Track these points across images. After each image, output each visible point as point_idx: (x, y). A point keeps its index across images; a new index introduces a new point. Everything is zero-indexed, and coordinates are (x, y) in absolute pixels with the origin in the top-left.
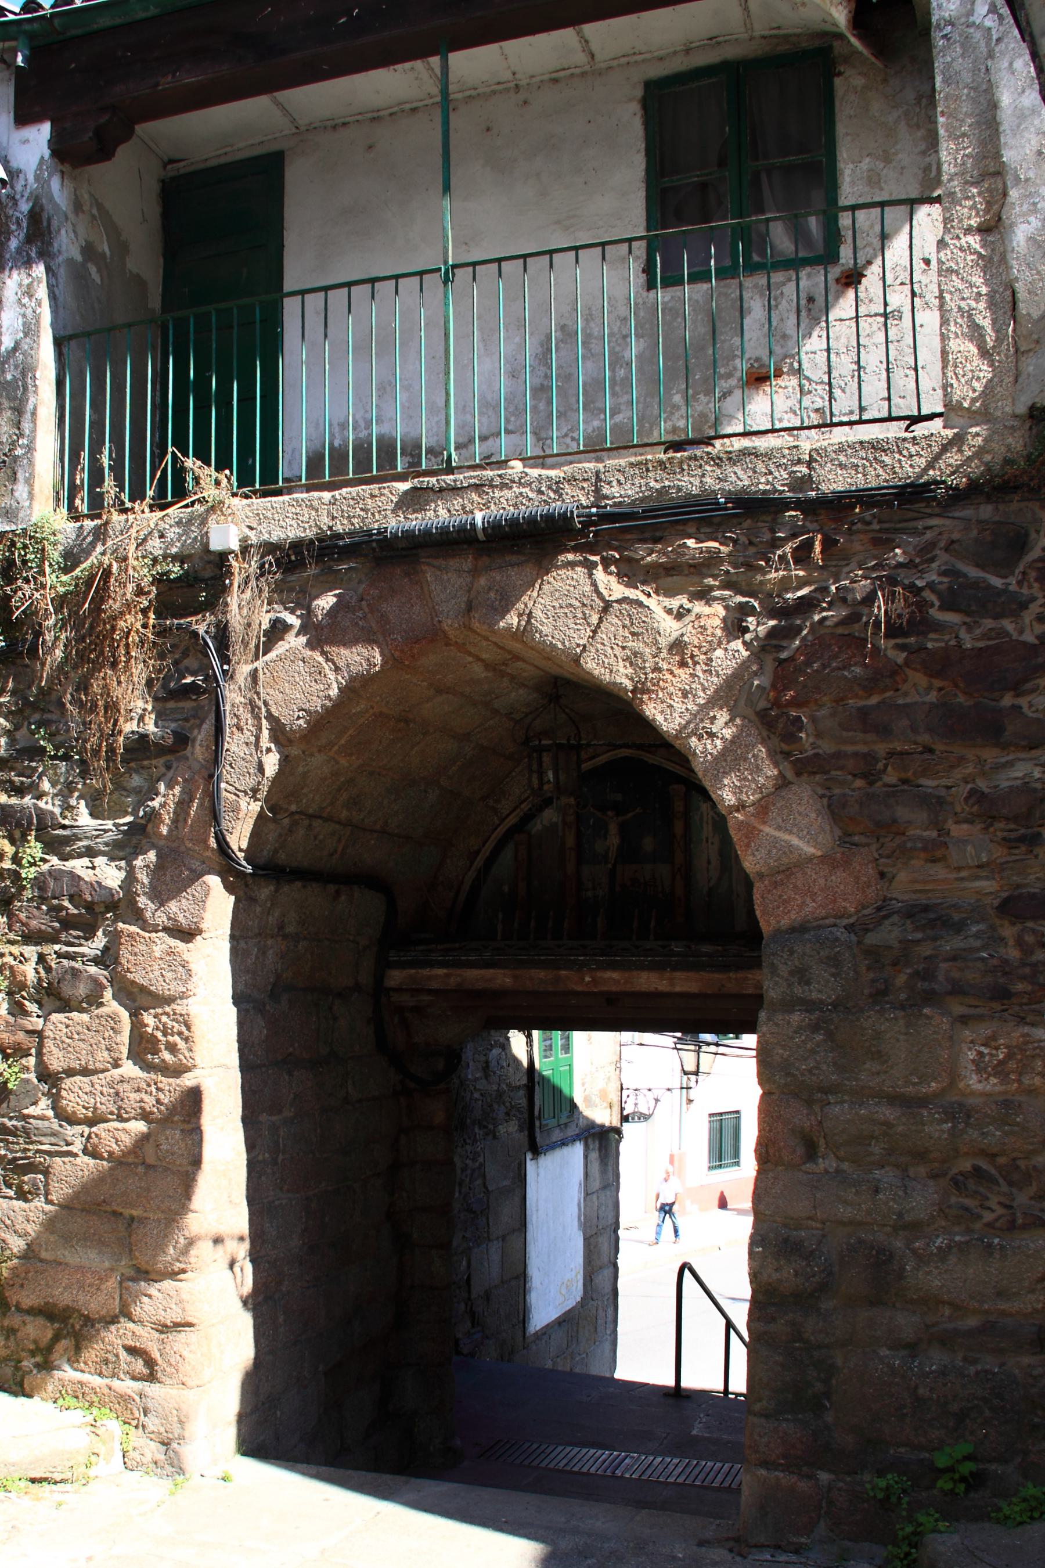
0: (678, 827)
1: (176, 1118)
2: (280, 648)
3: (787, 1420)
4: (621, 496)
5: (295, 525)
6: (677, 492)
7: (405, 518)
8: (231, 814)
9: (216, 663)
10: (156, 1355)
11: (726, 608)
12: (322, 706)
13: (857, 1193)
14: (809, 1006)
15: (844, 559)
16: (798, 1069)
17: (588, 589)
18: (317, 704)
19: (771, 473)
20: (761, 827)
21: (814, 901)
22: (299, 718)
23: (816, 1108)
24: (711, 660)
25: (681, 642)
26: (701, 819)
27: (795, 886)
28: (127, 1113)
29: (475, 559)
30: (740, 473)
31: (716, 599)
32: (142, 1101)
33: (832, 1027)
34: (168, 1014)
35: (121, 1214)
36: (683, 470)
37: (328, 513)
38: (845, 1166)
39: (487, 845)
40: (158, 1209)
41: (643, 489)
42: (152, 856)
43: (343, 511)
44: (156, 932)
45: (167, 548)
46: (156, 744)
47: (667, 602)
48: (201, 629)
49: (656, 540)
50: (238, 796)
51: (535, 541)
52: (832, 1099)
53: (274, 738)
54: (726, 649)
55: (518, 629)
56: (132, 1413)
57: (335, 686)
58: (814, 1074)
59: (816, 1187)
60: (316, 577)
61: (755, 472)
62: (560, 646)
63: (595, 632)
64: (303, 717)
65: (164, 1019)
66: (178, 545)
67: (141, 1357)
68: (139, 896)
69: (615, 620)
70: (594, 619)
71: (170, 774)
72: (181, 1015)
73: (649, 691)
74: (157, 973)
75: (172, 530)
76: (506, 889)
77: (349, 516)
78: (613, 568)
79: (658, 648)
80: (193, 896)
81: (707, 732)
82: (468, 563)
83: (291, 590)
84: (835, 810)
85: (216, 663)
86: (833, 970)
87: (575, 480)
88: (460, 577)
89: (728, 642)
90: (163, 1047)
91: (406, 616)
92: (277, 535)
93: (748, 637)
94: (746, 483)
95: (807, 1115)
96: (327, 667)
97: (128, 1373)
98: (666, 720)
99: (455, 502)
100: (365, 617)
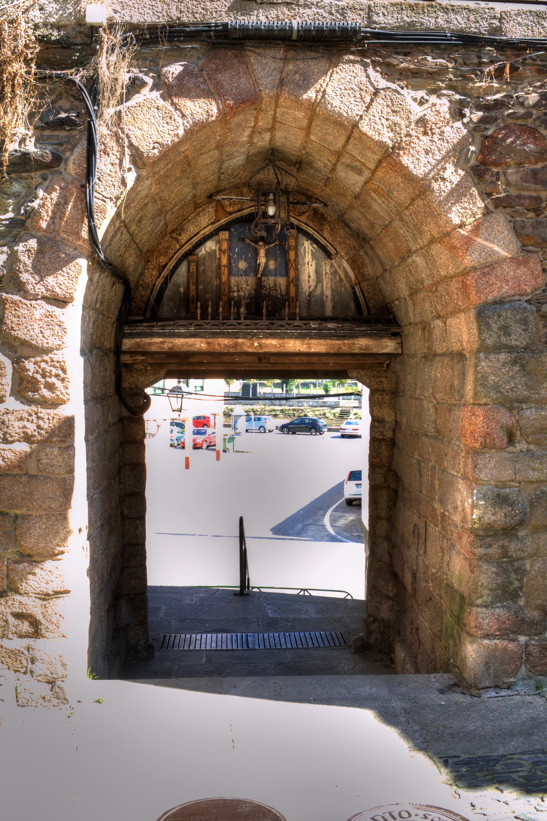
0: (292, 254)
1: (55, 439)
2: (137, 99)
3: (498, 607)
4: (385, 23)
5: (151, 14)
6: (421, 26)
7: (235, 18)
8: (99, 214)
9: (89, 103)
10: (39, 617)
11: (450, 101)
12: (172, 141)
13: (541, 463)
14: (510, 349)
15: (520, 80)
16: (504, 388)
17: (364, 79)
18: (168, 140)
19: (478, 22)
20: (475, 239)
21: (507, 285)
22: (154, 148)
23: (515, 412)
24: (443, 132)
25: (424, 119)
26: (305, 251)
27: (496, 276)
28: (11, 436)
29: (286, 52)
30: (460, 20)
31: (444, 95)
32: (24, 427)
33: (525, 362)
34: (46, 362)
35: (7, 514)
36: (424, 12)
37: (177, 8)
38: (532, 447)
40: (40, 508)
41: (399, 20)
42: (33, 243)
43: (188, 8)
44: (36, 300)
45: (46, 18)
46: (36, 161)
47: (413, 93)
48: (77, 79)
49: (406, 54)
50: (105, 202)
51: (330, 43)
52: (524, 406)
53: (134, 161)
54: (452, 127)
55: (315, 100)
56: (21, 663)
57: (182, 127)
58: (514, 391)
59: (516, 461)
60: (166, 51)
61: (469, 20)
62: (345, 115)
63: (368, 108)
64: (158, 148)
65: (43, 365)
66: (56, 17)
67: (27, 620)
68: (21, 272)
69: (382, 102)
70: (368, 99)
71: (46, 184)
72: (58, 362)
73: (403, 149)
74: (37, 331)
75: (51, 5)
76: (182, 290)
77: (193, 12)
78: (378, 68)
79: (410, 122)
80: (68, 273)
81: (440, 178)
82: (280, 53)
83: (145, 59)
84: (518, 231)
85: (89, 103)
86: (524, 327)
87: (355, 9)
88: (274, 62)
89: (453, 122)
90: (42, 386)
91: (236, 84)
92: (136, 19)
93: (465, 120)
94: (464, 26)
95: (510, 417)
96: (176, 115)
97: (16, 633)
98: (415, 167)
99: (272, 12)
100: (204, 82)
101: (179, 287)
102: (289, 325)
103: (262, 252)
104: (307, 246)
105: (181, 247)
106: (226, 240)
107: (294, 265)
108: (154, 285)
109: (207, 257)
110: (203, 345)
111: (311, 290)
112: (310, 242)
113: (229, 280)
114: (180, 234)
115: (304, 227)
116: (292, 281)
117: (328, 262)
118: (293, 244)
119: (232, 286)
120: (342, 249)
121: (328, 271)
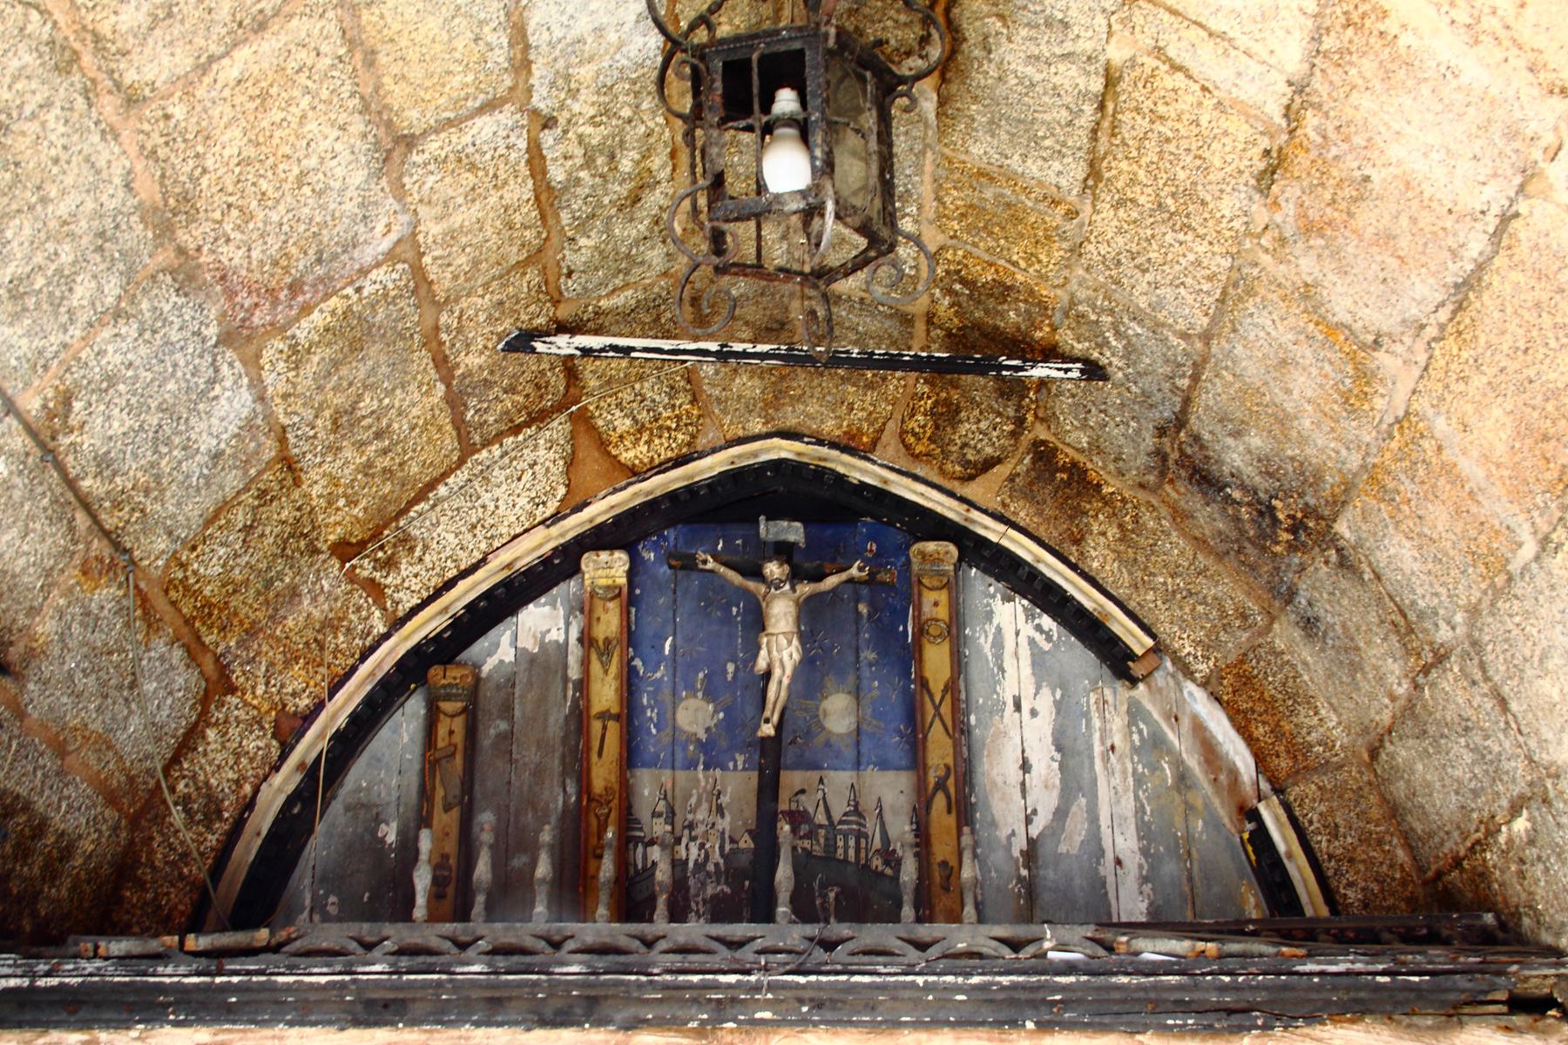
0: (936, 660)
26: (998, 644)
39: (340, 696)
101: (378, 820)
102: (922, 946)
103: (782, 613)
104: (1008, 622)
105: (397, 623)
106: (614, 593)
107: (946, 709)
108: (250, 805)
109: (522, 679)
111: (1034, 831)
112: (1021, 603)
113: (626, 791)
114: (390, 564)
115: (992, 531)
116: (941, 785)
117: (1117, 694)
118: (942, 613)
119: (643, 812)
120: (1183, 625)
121: (1117, 740)
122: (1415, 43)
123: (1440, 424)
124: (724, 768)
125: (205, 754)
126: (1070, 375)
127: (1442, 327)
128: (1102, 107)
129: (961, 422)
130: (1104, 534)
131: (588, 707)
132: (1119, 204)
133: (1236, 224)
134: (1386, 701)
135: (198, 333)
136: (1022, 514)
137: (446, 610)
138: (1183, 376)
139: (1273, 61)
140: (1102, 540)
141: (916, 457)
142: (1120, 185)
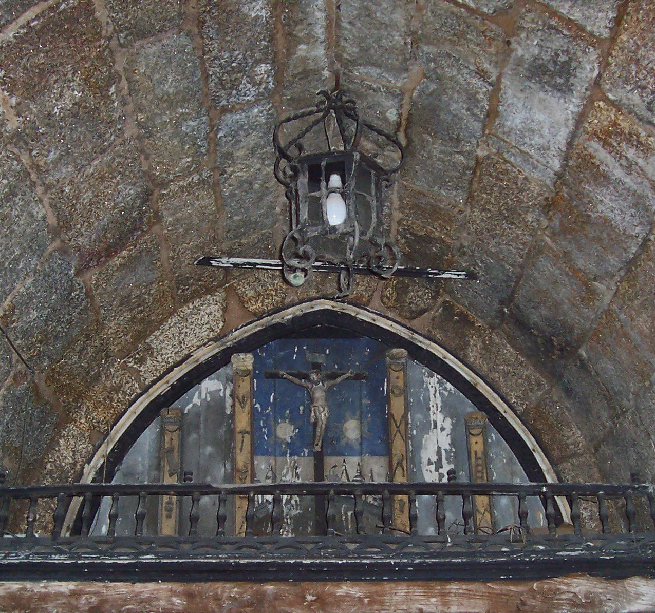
105: (145, 390)
107: (402, 428)
110: (176, 600)
112: (436, 378)
114: (141, 361)
115: (425, 344)
116: (400, 464)
118: (400, 383)
122: (606, 169)
123: (622, 316)
124: (299, 456)
125: (59, 451)
126: (460, 277)
127: (621, 277)
128: (474, 173)
129: (409, 292)
130: (476, 346)
131: (234, 428)
132: (484, 210)
133: (534, 224)
134: (601, 428)
135: (67, 274)
136: (438, 336)
137: (168, 382)
138: (512, 281)
139: (549, 165)
140: (475, 348)
141: (388, 308)
142: (482, 203)
